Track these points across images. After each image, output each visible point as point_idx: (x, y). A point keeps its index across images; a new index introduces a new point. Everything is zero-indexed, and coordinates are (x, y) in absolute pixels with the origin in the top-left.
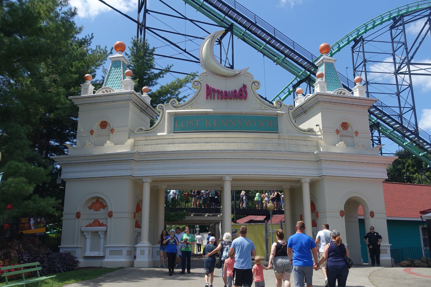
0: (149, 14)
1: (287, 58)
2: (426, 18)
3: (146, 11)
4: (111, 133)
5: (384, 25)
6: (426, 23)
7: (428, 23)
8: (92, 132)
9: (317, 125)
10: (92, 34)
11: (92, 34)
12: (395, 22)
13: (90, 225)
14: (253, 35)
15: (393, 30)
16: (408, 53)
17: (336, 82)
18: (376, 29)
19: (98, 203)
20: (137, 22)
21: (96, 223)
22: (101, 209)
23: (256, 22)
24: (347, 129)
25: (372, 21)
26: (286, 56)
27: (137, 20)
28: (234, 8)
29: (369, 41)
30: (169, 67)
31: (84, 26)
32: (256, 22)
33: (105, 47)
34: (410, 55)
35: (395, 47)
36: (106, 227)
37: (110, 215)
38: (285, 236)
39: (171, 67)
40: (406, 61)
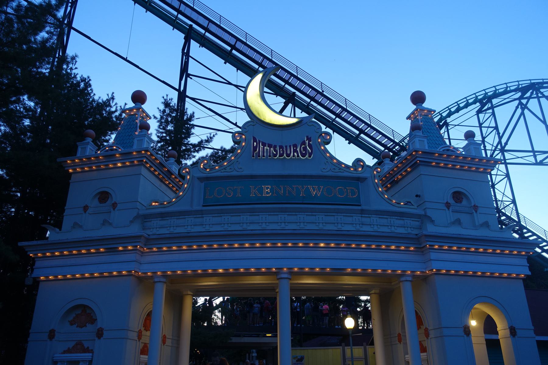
0: (191, 78)
1: (362, 135)
2: (517, 102)
3: (188, 75)
4: (112, 210)
5: (470, 108)
6: (517, 107)
7: (520, 107)
8: (86, 208)
9: (417, 196)
10: (113, 93)
11: (113, 93)
12: (483, 105)
13: (68, 351)
14: (319, 107)
15: (480, 115)
16: (500, 138)
17: (437, 139)
18: (461, 112)
19: (83, 314)
20: (178, 90)
21: (80, 347)
22: (87, 325)
23: (323, 91)
24: (461, 202)
25: (456, 104)
26: (361, 131)
27: (178, 88)
28: (296, 74)
29: (456, 125)
30: (212, 136)
31: (78, 54)
32: (323, 91)
33: (124, 104)
34: (504, 141)
35: (484, 132)
36: (91, 354)
37: (100, 334)
38: (104, 205)
39: (214, 136)
40: (499, 147)
